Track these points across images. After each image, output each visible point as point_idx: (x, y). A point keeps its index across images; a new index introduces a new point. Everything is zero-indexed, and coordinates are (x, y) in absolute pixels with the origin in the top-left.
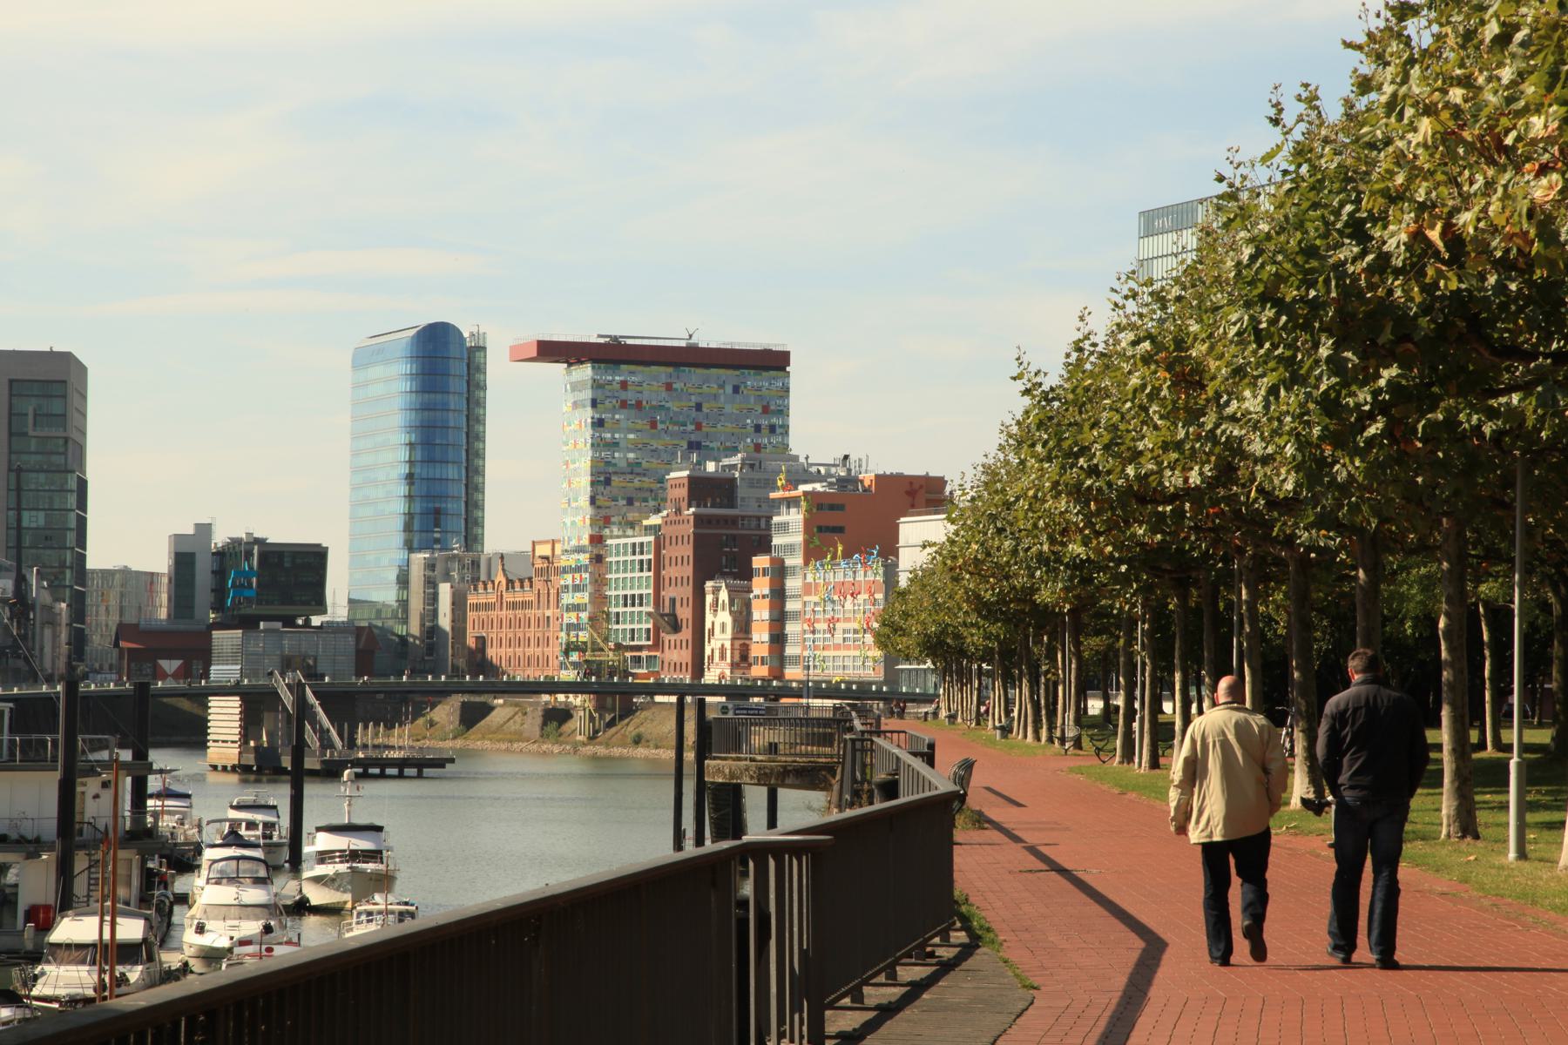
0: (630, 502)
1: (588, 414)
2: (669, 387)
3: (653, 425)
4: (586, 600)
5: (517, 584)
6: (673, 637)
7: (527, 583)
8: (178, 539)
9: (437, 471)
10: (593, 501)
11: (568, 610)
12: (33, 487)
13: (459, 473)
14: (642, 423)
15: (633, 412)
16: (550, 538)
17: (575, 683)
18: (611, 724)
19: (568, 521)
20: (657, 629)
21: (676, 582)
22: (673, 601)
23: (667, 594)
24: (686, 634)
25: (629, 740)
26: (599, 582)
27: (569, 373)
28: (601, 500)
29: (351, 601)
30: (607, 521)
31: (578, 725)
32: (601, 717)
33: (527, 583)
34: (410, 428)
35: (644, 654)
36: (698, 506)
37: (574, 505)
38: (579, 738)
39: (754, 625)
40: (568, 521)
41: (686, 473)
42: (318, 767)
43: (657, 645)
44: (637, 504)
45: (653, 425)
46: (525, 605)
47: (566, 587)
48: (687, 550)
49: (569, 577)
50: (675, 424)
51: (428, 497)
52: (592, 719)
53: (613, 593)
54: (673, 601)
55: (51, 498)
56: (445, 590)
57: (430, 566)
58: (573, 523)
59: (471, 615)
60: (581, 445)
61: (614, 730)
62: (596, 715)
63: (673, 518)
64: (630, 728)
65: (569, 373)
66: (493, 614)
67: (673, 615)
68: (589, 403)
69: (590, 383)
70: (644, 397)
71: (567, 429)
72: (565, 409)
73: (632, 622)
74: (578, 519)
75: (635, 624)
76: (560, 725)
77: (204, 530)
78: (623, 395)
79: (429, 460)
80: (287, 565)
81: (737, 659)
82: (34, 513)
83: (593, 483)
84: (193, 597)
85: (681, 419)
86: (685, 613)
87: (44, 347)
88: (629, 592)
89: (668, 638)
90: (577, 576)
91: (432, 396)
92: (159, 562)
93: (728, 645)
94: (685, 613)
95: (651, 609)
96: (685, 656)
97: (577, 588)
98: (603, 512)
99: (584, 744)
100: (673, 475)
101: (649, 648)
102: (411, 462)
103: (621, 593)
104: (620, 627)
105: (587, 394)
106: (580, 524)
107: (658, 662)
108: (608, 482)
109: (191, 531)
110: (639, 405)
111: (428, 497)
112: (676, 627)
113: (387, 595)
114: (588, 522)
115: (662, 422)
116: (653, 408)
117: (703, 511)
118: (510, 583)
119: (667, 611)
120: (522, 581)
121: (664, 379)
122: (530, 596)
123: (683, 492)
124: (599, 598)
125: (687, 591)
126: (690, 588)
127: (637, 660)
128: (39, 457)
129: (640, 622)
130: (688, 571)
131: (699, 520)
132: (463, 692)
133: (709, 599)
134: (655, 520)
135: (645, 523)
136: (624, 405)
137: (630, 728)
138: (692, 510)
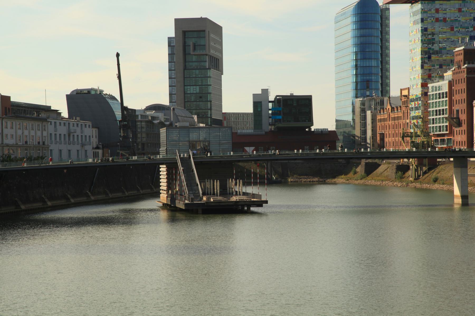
0: (441, 66)
1: (419, 26)
2: (460, 10)
3: (452, 29)
4: (420, 114)
5: (396, 109)
6: (458, 129)
7: (399, 108)
8: (254, 95)
9: (367, 63)
10: (422, 67)
11: (413, 119)
12: (194, 76)
13: (378, 63)
14: (446, 29)
15: (442, 23)
16: (407, 87)
17: (409, 152)
18: (425, 173)
19: (412, 77)
20: (451, 125)
21: (459, 102)
22: (458, 111)
23: (455, 108)
25: (432, 180)
26: (426, 106)
27: (412, 8)
29: (337, 121)
30: (430, 77)
31: (411, 173)
33: (399, 108)
34: (356, 45)
35: (446, 138)
36: (469, 63)
37: (414, 69)
38: (411, 179)
40: (412, 77)
41: (462, 48)
42: (183, 207)
43: (451, 133)
44: (444, 67)
45: (452, 29)
46: (399, 118)
47: (412, 108)
48: (463, 86)
49: (413, 103)
50: (463, 28)
51: (363, 75)
53: (431, 109)
54: (458, 111)
55: (202, 80)
56: (369, 113)
57: (363, 104)
58: (414, 78)
59: (378, 124)
60: (417, 41)
61: (427, 175)
63: (457, 70)
64: (434, 174)
65: (412, 8)
66: (387, 123)
67: (458, 118)
68: (420, 21)
69: (420, 11)
70: (447, 16)
71: (411, 34)
72: (410, 25)
73: (439, 123)
75: (439, 124)
76: (404, 173)
77: (265, 92)
78: (437, 16)
79: (364, 59)
80: (295, 104)
82: (195, 87)
83: (422, 58)
84: (261, 120)
85: (466, 25)
86: (463, 117)
87: (199, 17)
88: (438, 109)
89: (456, 129)
90: (416, 103)
91: (365, 30)
92: (247, 108)
94: (463, 117)
95: (447, 116)
97: (417, 109)
99: (412, 182)
100: (457, 49)
102: (356, 60)
103: (435, 109)
104: (435, 125)
105: (419, 17)
106: (417, 78)
107: (452, 142)
108: (429, 58)
109: (260, 92)
110: (445, 20)
111: (363, 75)
112: (459, 124)
113: (349, 118)
114: (420, 77)
115: (456, 27)
116: (452, 21)
117: (471, 66)
118: (393, 109)
119: (455, 116)
120: (397, 108)
121: (457, 6)
122: (400, 115)
123: (461, 57)
124: (426, 113)
125: (463, 106)
126: (465, 104)
127: (443, 141)
128: (196, 64)
129: (443, 122)
130: (464, 96)
131: (469, 70)
136: (437, 20)
137: (434, 174)
138: (466, 65)
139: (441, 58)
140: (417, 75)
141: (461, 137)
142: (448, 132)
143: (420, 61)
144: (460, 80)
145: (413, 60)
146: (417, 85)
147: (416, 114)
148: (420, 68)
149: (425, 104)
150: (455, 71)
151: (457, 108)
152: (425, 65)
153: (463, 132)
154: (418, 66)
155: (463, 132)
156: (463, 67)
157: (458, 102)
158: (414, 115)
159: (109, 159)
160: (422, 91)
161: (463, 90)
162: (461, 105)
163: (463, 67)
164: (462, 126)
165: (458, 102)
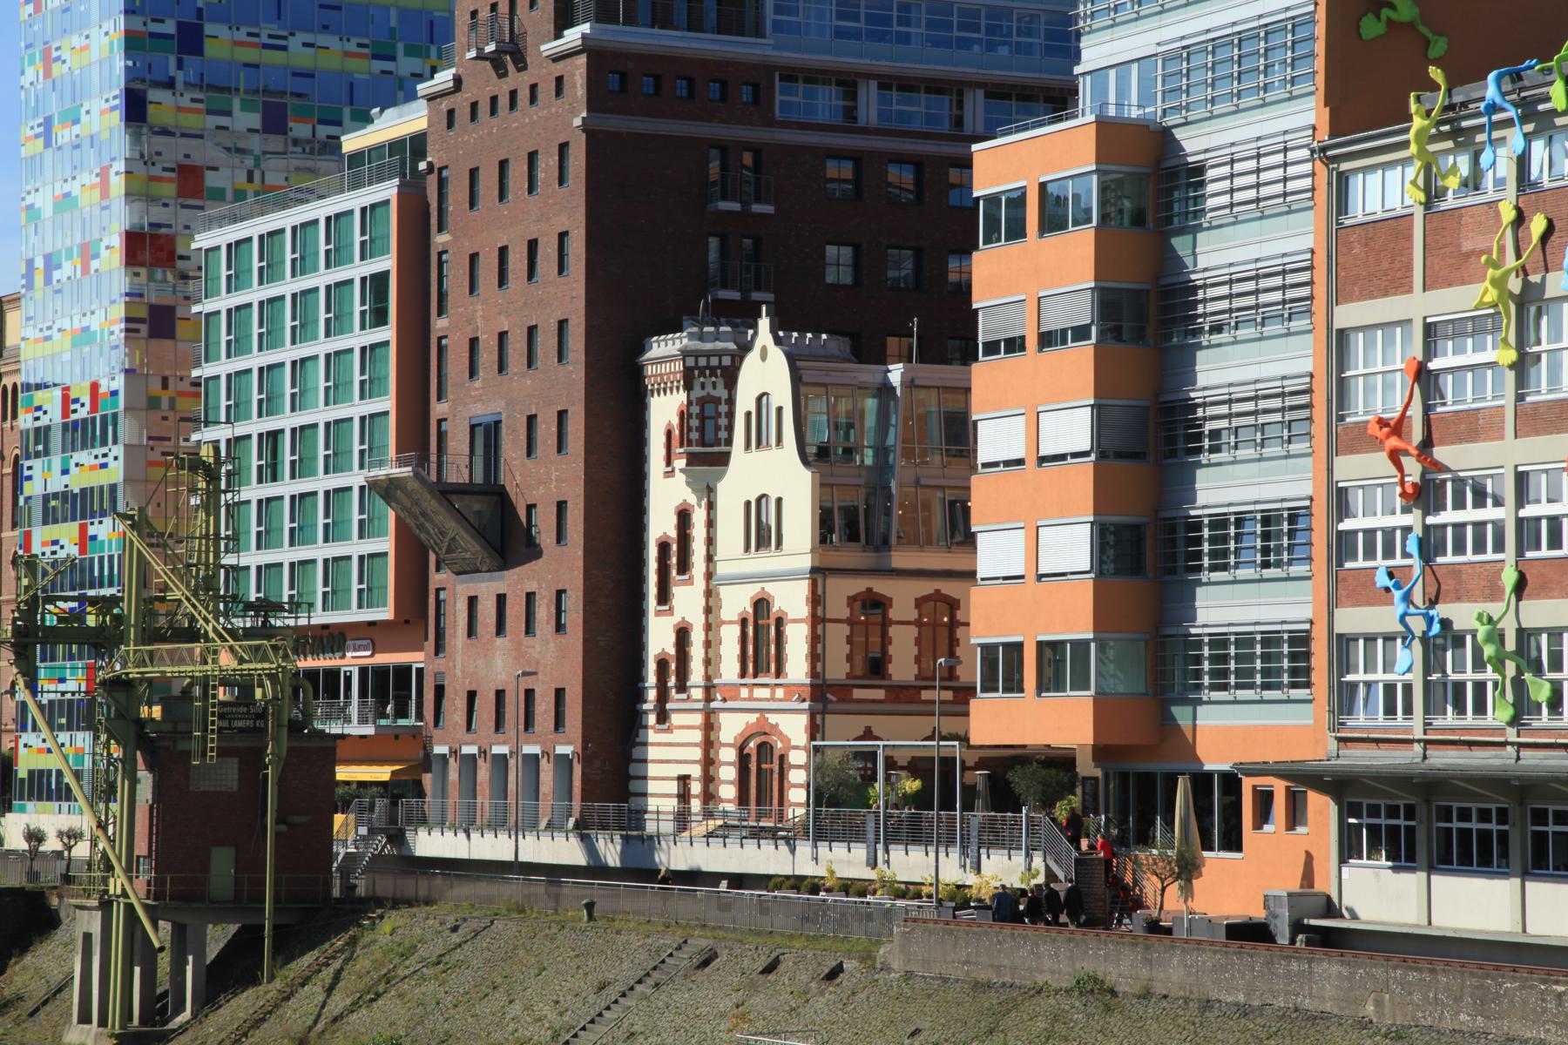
4: (115, 473)
6: (487, 588)
10: (135, 108)
18: (228, 976)
22: (488, 435)
23: (457, 411)
24: (561, 567)
28: (162, 105)
32: (182, 942)
35: (352, 661)
36: (604, 14)
37: (64, 135)
39: (983, 493)
40: (43, 201)
43: (417, 613)
47: (42, 434)
48: (563, 211)
52: (139, 950)
62: (160, 935)
74: (83, 186)
75: (321, 550)
81: (837, 669)
83: (133, 43)
86: (548, 481)
93: (792, 600)
94: (548, 481)
96: (557, 659)
98: (174, 151)
101: (371, 633)
106: (88, 199)
112: (506, 537)
114: (118, 184)
125: (564, 384)
130: (565, 296)
131: (609, 74)
132: (708, 627)
133: (664, 410)
134: (401, 122)
135: (352, 142)
139: (276, 57)
140: (89, 178)
141: (519, 653)
142: (385, 613)
143: (119, 64)
144: (518, 171)
145: (48, 60)
146: (88, 253)
147: (77, 481)
148: (117, 118)
149: (153, 403)
150: (461, 102)
151: (482, 411)
152: (153, 95)
153: (544, 612)
154: (97, 105)
155: (544, 612)
156: (550, 47)
157: (487, 356)
158: (57, 484)
159: (223, 704)
160: (133, 296)
161: (548, 250)
162: (519, 377)
163: (550, 47)
164: (532, 551)
165: (487, 356)
